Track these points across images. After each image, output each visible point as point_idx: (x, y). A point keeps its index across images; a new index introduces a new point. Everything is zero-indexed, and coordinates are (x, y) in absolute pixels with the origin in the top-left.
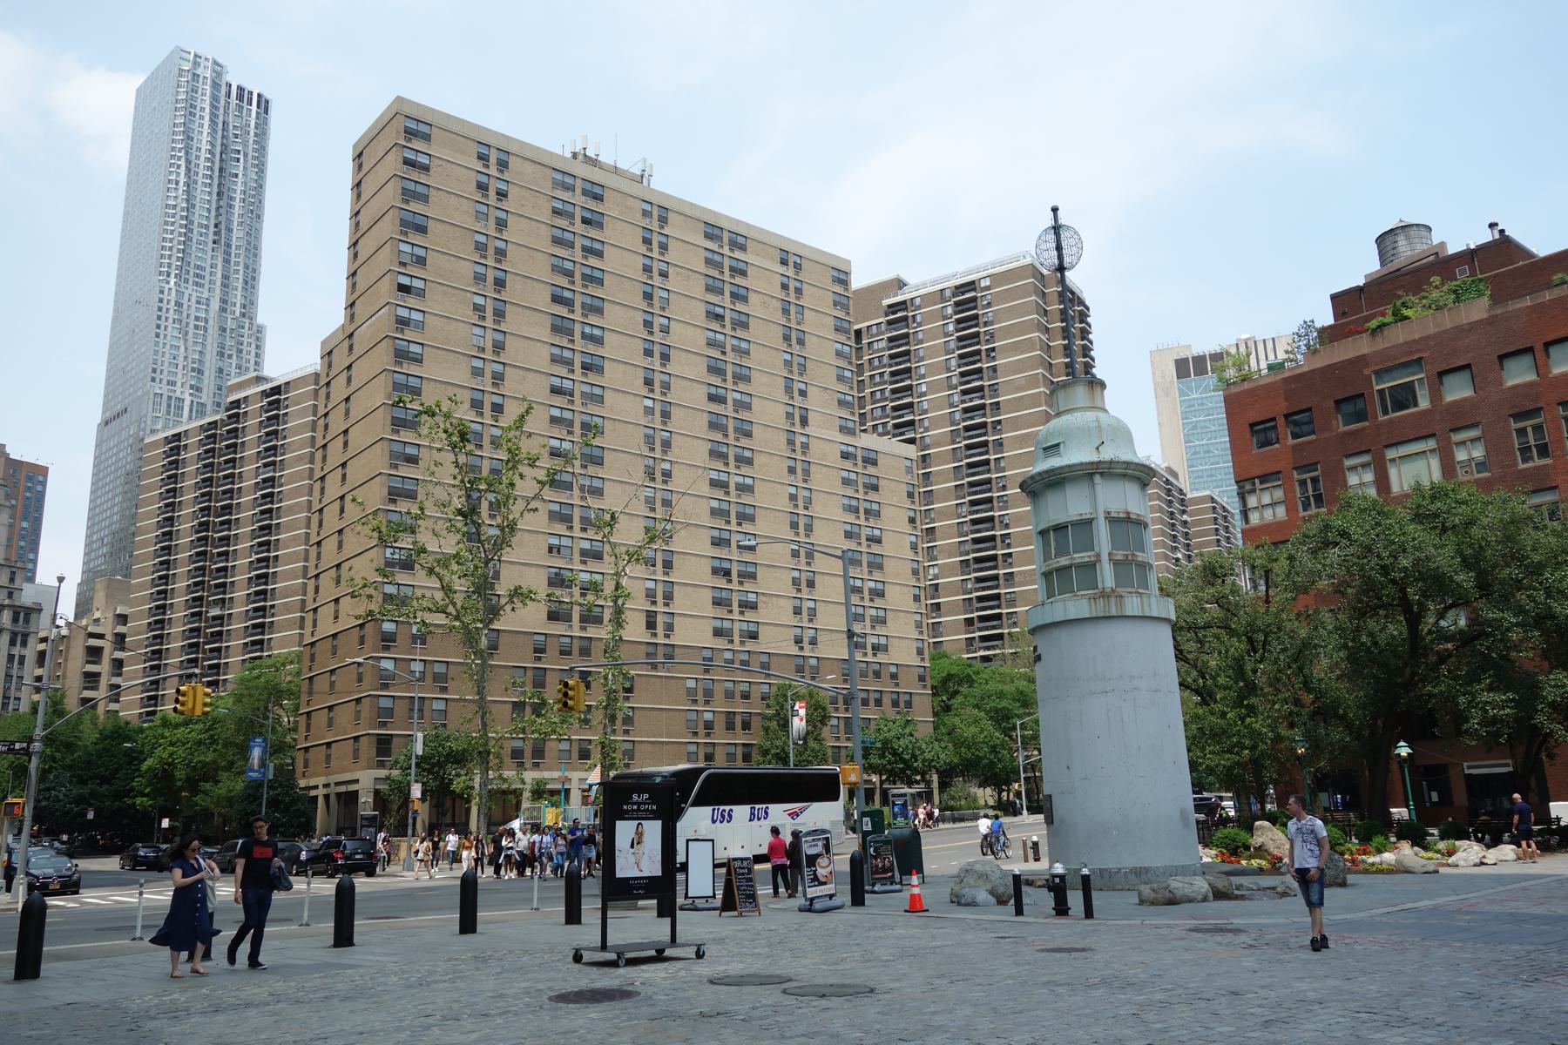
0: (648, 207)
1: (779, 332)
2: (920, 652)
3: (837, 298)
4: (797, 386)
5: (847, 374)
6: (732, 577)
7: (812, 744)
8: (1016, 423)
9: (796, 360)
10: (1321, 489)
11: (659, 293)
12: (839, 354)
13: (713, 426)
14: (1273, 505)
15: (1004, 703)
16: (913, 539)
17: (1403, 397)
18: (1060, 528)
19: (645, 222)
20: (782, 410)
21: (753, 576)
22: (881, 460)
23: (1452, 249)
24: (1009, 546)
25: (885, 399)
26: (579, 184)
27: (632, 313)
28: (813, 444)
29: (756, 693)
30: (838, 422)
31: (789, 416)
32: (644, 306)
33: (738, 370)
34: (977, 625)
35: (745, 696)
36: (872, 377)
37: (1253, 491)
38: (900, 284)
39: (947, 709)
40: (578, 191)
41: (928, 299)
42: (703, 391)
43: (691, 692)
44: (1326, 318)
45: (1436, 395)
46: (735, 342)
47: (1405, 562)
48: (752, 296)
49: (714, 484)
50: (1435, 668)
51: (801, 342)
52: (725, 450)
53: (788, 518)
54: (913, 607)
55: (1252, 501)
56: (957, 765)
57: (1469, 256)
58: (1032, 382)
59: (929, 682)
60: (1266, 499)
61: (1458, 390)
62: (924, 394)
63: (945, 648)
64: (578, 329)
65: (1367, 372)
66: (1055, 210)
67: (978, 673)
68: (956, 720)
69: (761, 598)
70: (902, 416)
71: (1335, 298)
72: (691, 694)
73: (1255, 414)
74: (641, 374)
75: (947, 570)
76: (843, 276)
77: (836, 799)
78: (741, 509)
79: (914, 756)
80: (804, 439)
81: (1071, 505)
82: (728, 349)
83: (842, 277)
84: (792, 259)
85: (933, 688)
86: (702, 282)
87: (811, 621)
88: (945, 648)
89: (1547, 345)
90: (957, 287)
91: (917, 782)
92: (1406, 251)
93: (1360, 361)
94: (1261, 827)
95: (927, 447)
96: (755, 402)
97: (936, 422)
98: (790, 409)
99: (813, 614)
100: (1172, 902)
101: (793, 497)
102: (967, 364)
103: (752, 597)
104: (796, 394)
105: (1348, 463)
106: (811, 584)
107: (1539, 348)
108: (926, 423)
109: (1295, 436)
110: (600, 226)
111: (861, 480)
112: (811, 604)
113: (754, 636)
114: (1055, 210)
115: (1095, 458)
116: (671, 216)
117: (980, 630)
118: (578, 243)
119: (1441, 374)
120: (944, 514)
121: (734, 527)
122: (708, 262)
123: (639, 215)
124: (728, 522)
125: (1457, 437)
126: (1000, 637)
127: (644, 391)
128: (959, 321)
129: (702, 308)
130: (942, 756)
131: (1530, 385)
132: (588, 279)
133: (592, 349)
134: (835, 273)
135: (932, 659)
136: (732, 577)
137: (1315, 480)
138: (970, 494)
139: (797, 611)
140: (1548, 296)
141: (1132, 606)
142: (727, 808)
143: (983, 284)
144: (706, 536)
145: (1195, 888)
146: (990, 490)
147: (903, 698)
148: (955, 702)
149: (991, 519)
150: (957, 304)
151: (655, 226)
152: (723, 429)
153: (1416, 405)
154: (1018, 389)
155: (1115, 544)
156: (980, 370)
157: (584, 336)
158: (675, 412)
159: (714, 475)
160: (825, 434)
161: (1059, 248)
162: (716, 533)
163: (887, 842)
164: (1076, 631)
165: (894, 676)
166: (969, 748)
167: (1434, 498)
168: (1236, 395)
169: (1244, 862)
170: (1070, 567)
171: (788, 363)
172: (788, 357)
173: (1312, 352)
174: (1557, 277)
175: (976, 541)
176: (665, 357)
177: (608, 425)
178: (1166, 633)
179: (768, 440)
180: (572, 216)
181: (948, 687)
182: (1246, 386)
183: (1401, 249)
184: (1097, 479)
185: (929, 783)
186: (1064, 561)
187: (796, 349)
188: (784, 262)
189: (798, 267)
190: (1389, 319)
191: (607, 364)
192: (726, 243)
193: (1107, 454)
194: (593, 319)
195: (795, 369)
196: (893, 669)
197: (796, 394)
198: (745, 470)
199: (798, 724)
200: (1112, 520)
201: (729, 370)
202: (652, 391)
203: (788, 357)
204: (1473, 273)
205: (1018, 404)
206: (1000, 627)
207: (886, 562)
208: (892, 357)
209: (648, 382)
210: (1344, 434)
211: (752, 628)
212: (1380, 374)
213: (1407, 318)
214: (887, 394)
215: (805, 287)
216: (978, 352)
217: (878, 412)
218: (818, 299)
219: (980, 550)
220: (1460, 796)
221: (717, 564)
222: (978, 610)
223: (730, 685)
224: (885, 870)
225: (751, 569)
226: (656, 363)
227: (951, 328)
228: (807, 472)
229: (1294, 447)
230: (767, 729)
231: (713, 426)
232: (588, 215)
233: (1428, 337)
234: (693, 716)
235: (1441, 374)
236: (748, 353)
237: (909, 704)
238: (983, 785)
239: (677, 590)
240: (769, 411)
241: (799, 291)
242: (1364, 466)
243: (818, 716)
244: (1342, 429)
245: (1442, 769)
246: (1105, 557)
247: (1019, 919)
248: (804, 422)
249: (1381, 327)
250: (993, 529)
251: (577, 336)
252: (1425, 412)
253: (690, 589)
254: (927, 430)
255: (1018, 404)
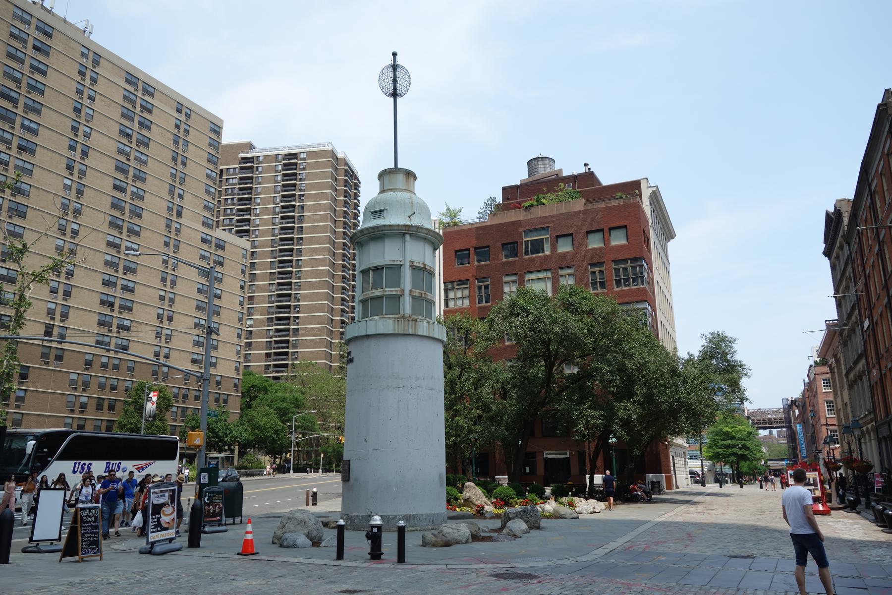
0: (86, 51)
1: (170, 155)
2: (237, 369)
3: (212, 142)
4: (177, 191)
5: (212, 190)
6: (115, 308)
7: (157, 423)
8: (311, 241)
9: (179, 175)
10: (488, 292)
11: (85, 110)
12: (208, 176)
13: (114, 206)
14: (463, 298)
15: (285, 405)
16: (242, 299)
17: (537, 247)
18: (377, 269)
19: (83, 61)
20: (165, 205)
21: (130, 309)
22: (227, 247)
23: (565, 173)
24: (298, 312)
25: (233, 215)
26: (34, 22)
27: (66, 119)
28: (183, 229)
29: (121, 387)
30: (202, 219)
31: (170, 209)
32: (74, 116)
33: (138, 173)
34: (273, 357)
35: (114, 388)
36: (226, 200)
37: (452, 289)
38: (251, 147)
39: (249, 406)
40: (33, 26)
41: (267, 158)
42: (110, 182)
43: (75, 382)
44: (499, 199)
45: (554, 248)
46: (138, 154)
47: (558, 329)
48: (153, 127)
49: (110, 244)
50: (559, 394)
51: (184, 164)
52: (121, 223)
53: (160, 275)
54: (236, 341)
55: (451, 295)
56: (252, 441)
57: (573, 179)
58: (323, 218)
59: (240, 389)
60: (459, 294)
61: (565, 247)
62: (257, 215)
63: (251, 369)
64: (18, 121)
65: (520, 230)
66: (394, 54)
67: (271, 386)
68: (255, 413)
69: (134, 324)
70: (242, 226)
71: (506, 190)
72: (73, 384)
73: (459, 245)
74: (65, 161)
75: (259, 323)
76: (217, 129)
77: (174, 459)
78: (127, 264)
79: (226, 435)
80: (178, 226)
81: (388, 253)
82: (132, 157)
83: (216, 129)
84: (184, 110)
85: (242, 393)
86: (119, 110)
87: (167, 342)
88: (251, 369)
89: (610, 229)
90: (286, 155)
91: (226, 451)
92: (542, 171)
93: (517, 224)
94: (469, 486)
95: (256, 247)
96: (147, 196)
97: (263, 233)
98: (171, 205)
99: (169, 338)
100: (447, 544)
101: (165, 262)
102: (286, 201)
103: (127, 323)
104: (176, 196)
105: (506, 279)
106: (170, 319)
107: (606, 230)
108: (257, 233)
109: (478, 261)
110: (47, 54)
111: (213, 258)
112: (169, 332)
113: (125, 348)
114: (394, 54)
115: (408, 223)
116: (102, 62)
117: (274, 360)
118: (28, 61)
119: (558, 237)
120: (261, 289)
121: (120, 275)
122: (125, 97)
123: (78, 55)
124: (117, 271)
125: (562, 272)
126: (286, 366)
127: (65, 173)
128: (284, 175)
129: (117, 128)
130: (244, 435)
131: (600, 249)
132: (31, 88)
133: (28, 136)
134: (213, 126)
135: (244, 375)
136: (115, 308)
137: (487, 287)
138: (278, 279)
139: (158, 336)
140: (613, 203)
141: (423, 328)
142: (87, 462)
143: (302, 156)
144: (99, 278)
145: (462, 533)
146: (291, 278)
147: (222, 397)
148: (255, 403)
149: (290, 295)
150: (285, 165)
151: (90, 65)
152: (122, 210)
153: (543, 251)
154: (315, 221)
155: (415, 285)
156: (294, 206)
157: (23, 126)
158: (87, 192)
159: (111, 239)
160: (192, 223)
161: (395, 81)
162: (107, 277)
163: (218, 493)
164: (382, 343)
165: (218, 383)
166: (262, 431)
167: (571, 295)
168: (450, 233)
169: (458, 510)
170: (381, 297)
171: (173, 176)
172: (174, 171)
173: (493, 214)
174: (618, 195)
175: (278, 307)
176: (85, 154)
177: (33, 192)
178: (439, 350)
179: (153, 221)
180: (25, 42)
181: (251, 393)
182: (456, 228)
183: (540, 169)
184: (408, 238)
185: (232, 452)
186: (378, 293)
187: (180, 167)
188: (179, 111)
189: (188, 116)
190: (535, 203)
191: (38, 149)
192: (140, 92)
193: (416, 221)
194: (31, 116)
195: (178, 180)
196: (218, 379)
197: (176, 196)
198: (133, 239)
199: (150, 407)
200: (414, 268)
201: (131, 171)
202: (72, 174)
203: (174, 171)
204: (574, 188)
205: (314, 230)
206: (287, 360)
207: (222, 311)
208: (240, 189)
209: (70, 168)
210: (505, 263)
211: (125, 343)
212: (527, 232)
213: (543, 204)
214: (234, 211)
215: (191, 129)
216: (294, 195)
217: (228, 222)
218: (198, 139)
219: (280, 313)
220: (541, 470)
221: (105, 298)
222: (274, 348)
223: (104, 380)
224: (215, 514)
225: (129, 304)
226: (77, 156)
227: (279, 178)
228: (177, 247)
229: (478, 266)
230: (126, 411)
231: (114, 206)
232: (39, 45)
233: (553, 216)
234: (72, 399)
235: (558, 237)
236: (146, 163)
237: (226, 401)
238: (266, 454)
239: (72, 312)
240: (155, 203)
241: (186, 132)
242: (513, 282)
243: (164, 404)
244: (504, 260)
245: (533, 455)
246: (407, 293)
247: (340, 563)
248: (179, 214)
249: (531, 206)
250: (290, 301)
251: (18, 125)
252: (548, 256)
253: (82, 312)
254: (257, 236)
255: (314, 230)
